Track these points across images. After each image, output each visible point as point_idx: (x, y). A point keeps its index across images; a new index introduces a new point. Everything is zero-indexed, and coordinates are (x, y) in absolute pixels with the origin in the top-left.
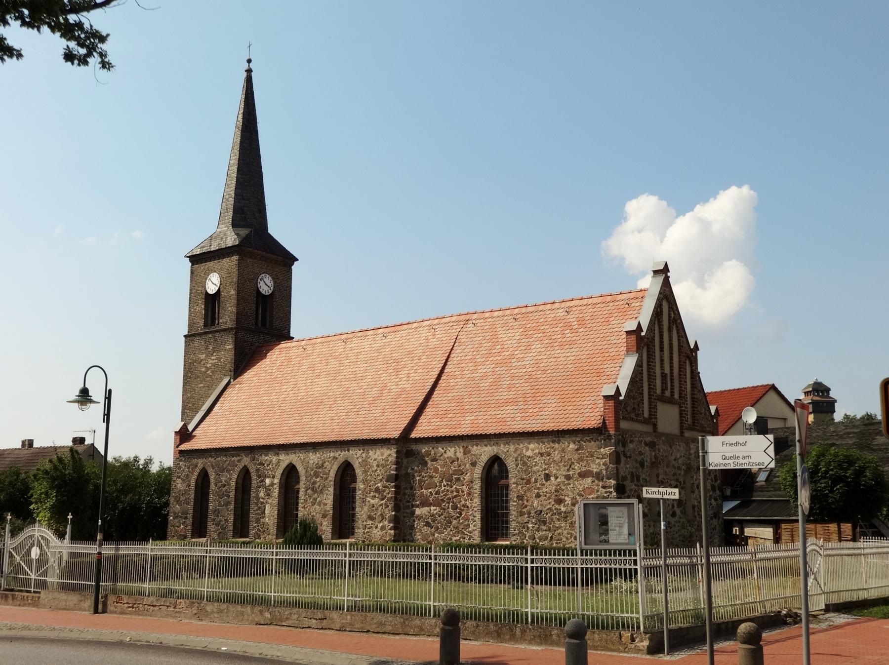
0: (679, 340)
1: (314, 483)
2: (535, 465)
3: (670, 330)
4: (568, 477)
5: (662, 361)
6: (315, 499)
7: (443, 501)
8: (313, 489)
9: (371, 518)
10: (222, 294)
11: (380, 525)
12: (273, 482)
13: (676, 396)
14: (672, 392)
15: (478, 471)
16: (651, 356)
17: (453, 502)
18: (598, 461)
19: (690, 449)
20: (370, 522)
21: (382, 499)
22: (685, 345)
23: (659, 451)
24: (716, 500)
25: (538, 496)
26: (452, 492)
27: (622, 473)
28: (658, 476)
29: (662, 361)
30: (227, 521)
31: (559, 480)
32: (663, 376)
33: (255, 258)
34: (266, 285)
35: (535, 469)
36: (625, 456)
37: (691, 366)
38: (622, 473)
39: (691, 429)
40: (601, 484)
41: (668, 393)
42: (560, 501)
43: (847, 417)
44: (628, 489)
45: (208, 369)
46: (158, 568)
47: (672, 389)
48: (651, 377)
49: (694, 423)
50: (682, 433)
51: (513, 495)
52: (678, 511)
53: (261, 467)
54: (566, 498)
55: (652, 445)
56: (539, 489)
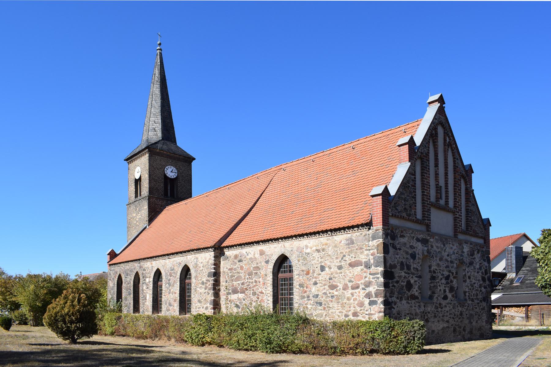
0: (454, 161)
1: (169, 280)
2: (313, 260)
3: (445, 152)
4: (340, 268)
5: (437, 175)
6: (170, 290)
7: (247, 289)
8: (169, 283)
9: (200, 301)
11: (205, 306)
12: (149, 280)
13: (451, 204)
14: (447, 202)
15: (271, 266)
16: (425, 168)
17: (253, 290)
18: (366, 252)
20: (199, 304)
21: (205, 289)
23: (432, 247)
24: (485, 288)
25: (315, 283)
26: (252, 283)
27: (389, 262)
28: (430, 267)
29: (437, 175)
30: (130, 303)
31: (332, 270)
32: (438, 188)
33: (162, 156)
34: (171, 172)
35: (313, 262)
36: (394, 247)
37: (466, 184)
38: (389, 262)
39: (463, 233)
41: (442, 202)
44: (396, 275)
45: (137, 222)
47: (447, 197)
48: (425, 185)
49: (467, 229)
50: (455, 235)
51: (296, 284)
52: (450, 296)
53: (144, 272)
54: (339, 284)
55: (425, 242)
56: (316, 278)
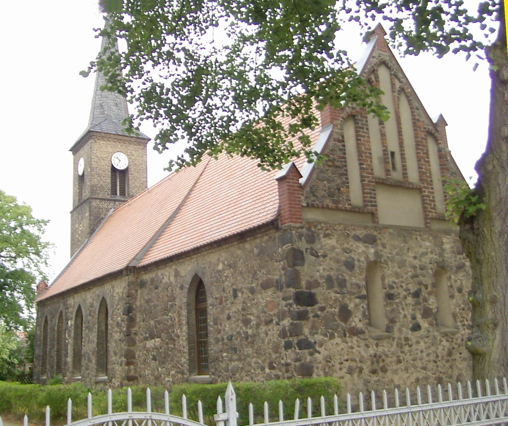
4: (252, 291)
10: (129, 170)
19: (442, 243)
22: (423, 119)
25: (229, 318)
40: (281, 294)
42: (246, 322)
43: (103, 11)
46: (274, 412)
